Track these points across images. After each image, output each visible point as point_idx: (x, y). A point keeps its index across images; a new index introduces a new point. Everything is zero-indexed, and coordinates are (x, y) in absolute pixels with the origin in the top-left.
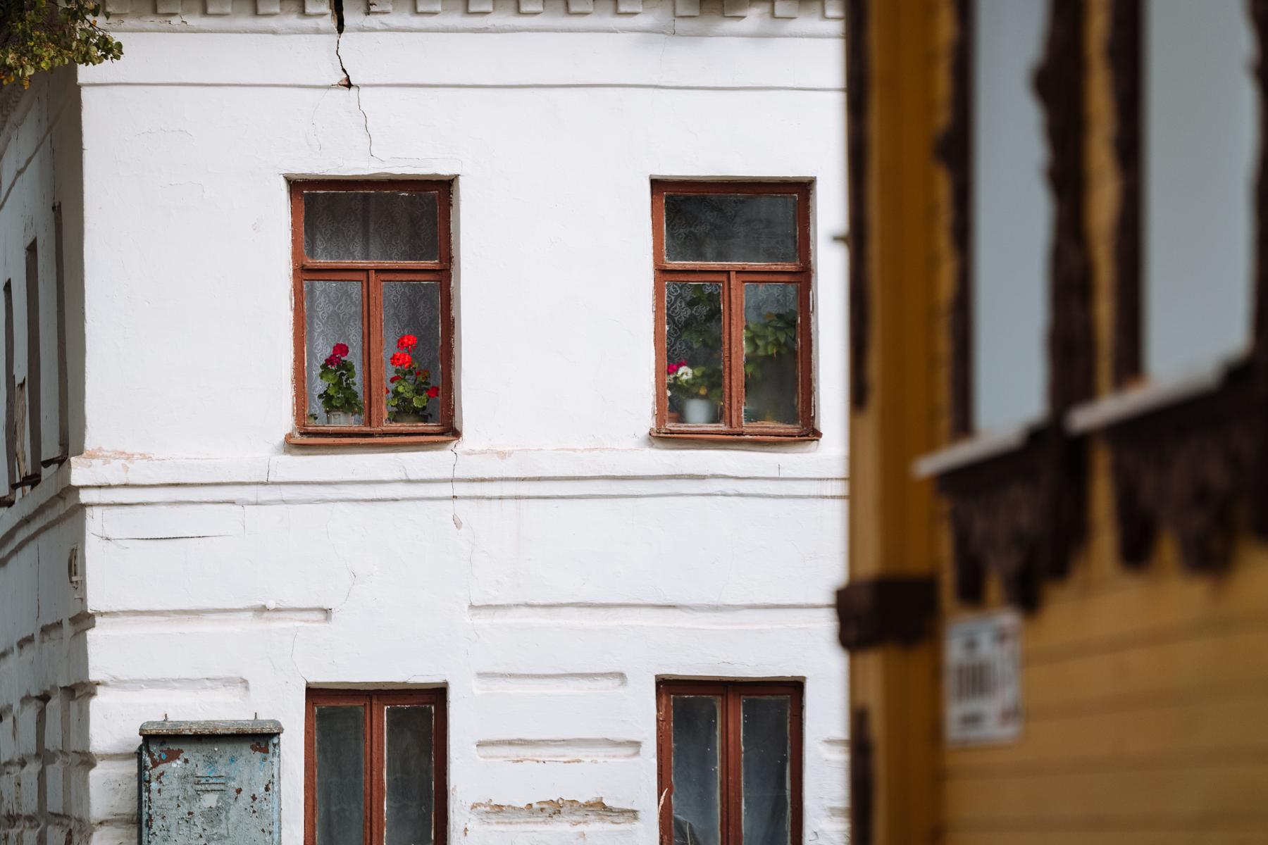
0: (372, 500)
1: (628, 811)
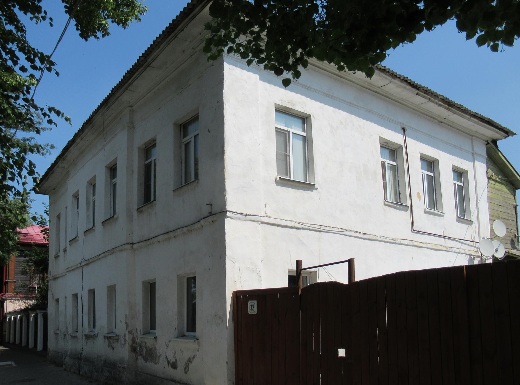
0: (111, 202)
1: (189, 288)
